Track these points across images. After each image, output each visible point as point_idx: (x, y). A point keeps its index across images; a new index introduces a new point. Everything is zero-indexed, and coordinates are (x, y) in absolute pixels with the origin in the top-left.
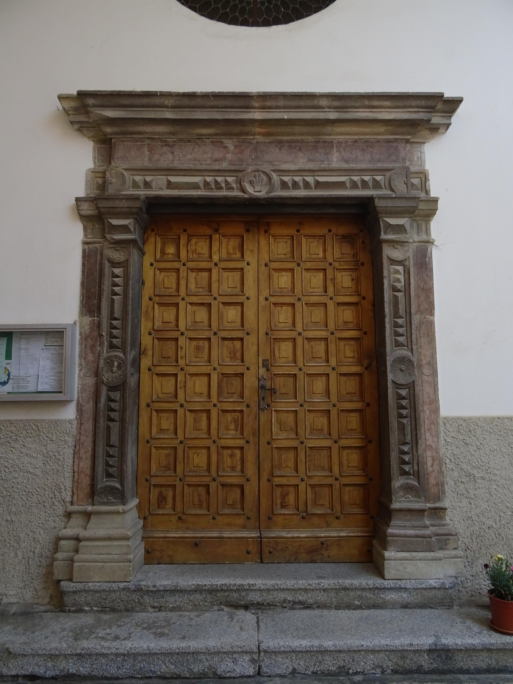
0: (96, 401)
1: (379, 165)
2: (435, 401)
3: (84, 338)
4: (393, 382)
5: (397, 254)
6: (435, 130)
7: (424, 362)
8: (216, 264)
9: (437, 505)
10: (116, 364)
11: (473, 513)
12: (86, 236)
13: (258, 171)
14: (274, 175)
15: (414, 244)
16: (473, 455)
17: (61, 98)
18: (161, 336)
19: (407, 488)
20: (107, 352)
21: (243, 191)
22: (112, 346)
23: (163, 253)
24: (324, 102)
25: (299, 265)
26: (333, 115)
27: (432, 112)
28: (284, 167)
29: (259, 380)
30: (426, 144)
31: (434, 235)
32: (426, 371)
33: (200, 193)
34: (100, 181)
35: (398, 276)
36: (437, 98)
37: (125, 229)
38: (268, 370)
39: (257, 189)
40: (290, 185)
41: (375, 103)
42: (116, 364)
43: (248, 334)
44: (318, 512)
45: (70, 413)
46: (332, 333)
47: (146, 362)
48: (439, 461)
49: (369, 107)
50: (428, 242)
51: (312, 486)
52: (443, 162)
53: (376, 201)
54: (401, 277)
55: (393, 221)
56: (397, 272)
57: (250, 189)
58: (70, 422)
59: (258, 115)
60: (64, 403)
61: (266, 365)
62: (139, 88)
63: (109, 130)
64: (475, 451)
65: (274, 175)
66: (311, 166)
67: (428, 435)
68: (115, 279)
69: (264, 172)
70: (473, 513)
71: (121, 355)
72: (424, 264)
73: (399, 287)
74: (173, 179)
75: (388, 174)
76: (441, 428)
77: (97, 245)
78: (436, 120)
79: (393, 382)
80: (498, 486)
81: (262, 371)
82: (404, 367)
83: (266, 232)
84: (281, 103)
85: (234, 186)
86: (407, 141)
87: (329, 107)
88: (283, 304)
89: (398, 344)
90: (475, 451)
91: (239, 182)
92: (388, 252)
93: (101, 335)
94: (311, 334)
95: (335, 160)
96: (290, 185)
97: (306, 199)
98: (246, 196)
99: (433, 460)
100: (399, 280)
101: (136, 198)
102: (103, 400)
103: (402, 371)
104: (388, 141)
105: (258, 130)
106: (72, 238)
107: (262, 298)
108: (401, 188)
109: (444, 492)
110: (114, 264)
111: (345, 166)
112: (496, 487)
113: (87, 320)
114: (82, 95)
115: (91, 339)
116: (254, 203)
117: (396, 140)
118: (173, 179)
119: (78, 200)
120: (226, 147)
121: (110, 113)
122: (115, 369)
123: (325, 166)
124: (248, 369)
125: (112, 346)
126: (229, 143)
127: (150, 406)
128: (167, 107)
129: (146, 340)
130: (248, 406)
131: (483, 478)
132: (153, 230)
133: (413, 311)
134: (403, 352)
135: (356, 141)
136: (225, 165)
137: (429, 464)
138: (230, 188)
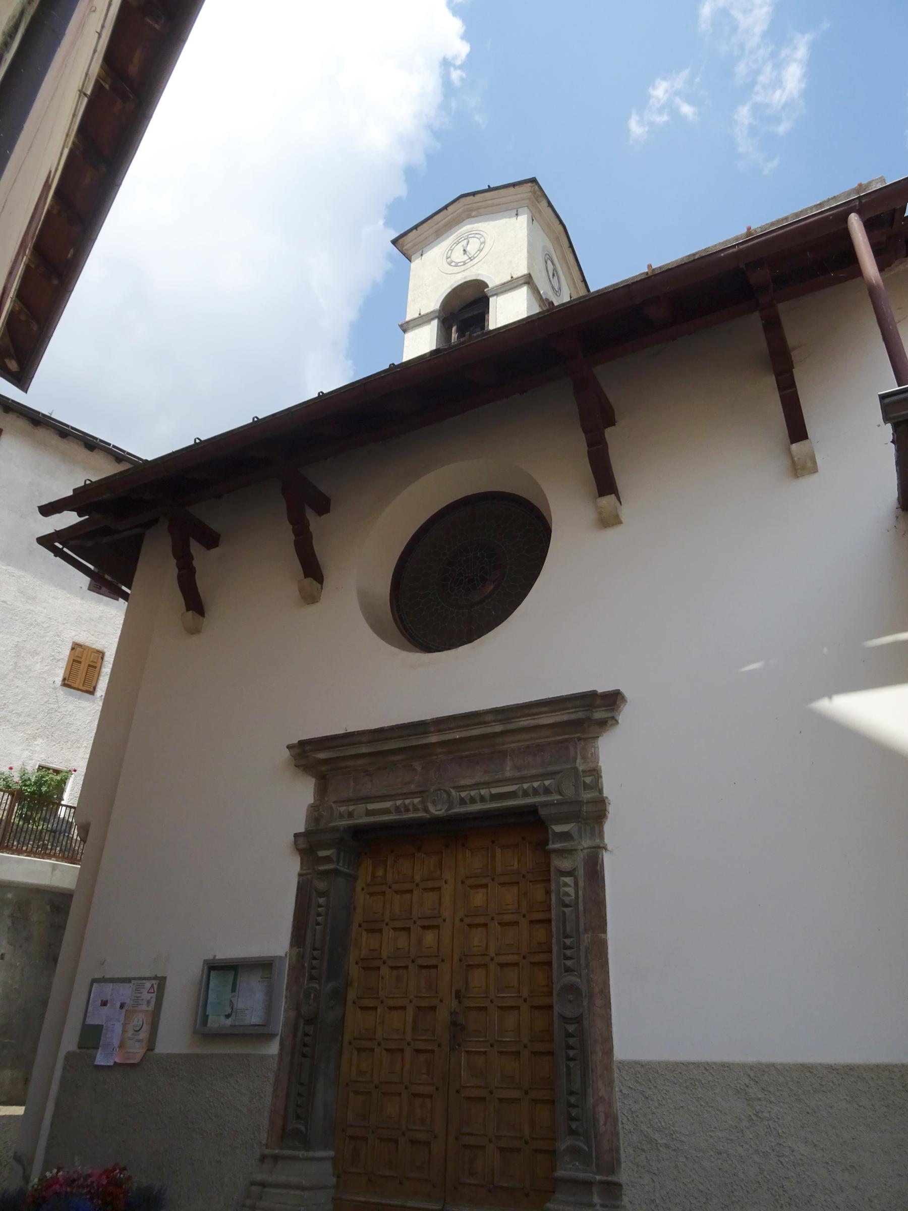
0: (295, 1036)
1: (550, 769)
2: (608, 1039)
3: (292, 969)
4: (560, 1015)
5: (565, 864)
6: (604, 724)
7: (596, 990)
8: (417, 885)
9: (610, 1178)
10: (312, 996)
11: (657, 1195)
12: (301, 868)
13: (439, 790)
14: (453, 792)
15: (585, 851)
16: (654, 1113)
17: (289, 747)
18: (370, 965)
19: (574, 1151)
20: (308, 984)
21: (426, 810)
22: (312, 978)
23: (374, 876)
24: (489, 718)
25: (493, 880)
26: (498, 728)
27: (595, 711)
28: (463, 782)
29: (451, 1014)
30: (600, 739)
31: (607, 839)
32: (599, 1002)
33: (391, 818)
34: (315, 813)
35: (567, 889)
36: (589, 700)
37: (328, 859)
38: (460, 1002)
39: (439, 808)
40: (468, 801)
41: (534, 711)
42: (312, 996)
43: (443, 961)
44: (505, 1185)
45: (274, 1048)
46: (524, 958)
47: (352, 995)
48: (612, 1118)
49: (529, 715)
50: (599, 847)
51: (502, 1150)
52: (615, 757)
53: (540, 809)
54: (571, 891)
55: (558, 828)
56: (566, 885)
57: (432, 809)
58: (273, 1056)
59: (434, 739)
60: (270, 1037)
61: (458, 995)
62: (340, 731)
63: (323, 768)
64: (656, 1108)
65: (453, 792)
66: (486, 778)
67: (600, 1084)
68: (320, 909)
69: (445, 791)
70: (657, 1195)
71: (317, 986)
72: (594, 873)
73: (567, 902)
74: (371, 806)
75: (558, 776)
76: (616, 1075)
77: (309, 876)
78: (598, 715)
79: (560, 1015)
80: (687, 1158)
81: (454, 1004)
82: (571, 997)
83: (463, 845)
84: (452, 725)
85: (420, 807)
86: (579, 739)
87: (494, 721)
88: (478, 925)
89: (568, 970)
90: (656, 1108)
91: (423, 802)
92: (559, 863)
93: (303, 967)
94: (503, 959)
95: (508, 769)
96: (468, 801)
97: (479, 812)
98: (428, 816)
99: (607, 1117)
100: (567, 894)
101: (335, 830)
102: (300, 1034)
103: (571, 1002)
104: (560, 742)
105: (439, 750)
106: (290, 869)
107: (457, 920)
108: (569, 792)
109: (619, 1162)
110: (321, 894)
111: (517, 774)
112: (684, 1160)
113: (296, 950)
114: (302, 743)
115: (296, 971)
116: (436, 822)
117: (567, 740)
118: (371, 806)
119: (296, 835)
120: (414, 770)
121: (321, 756)
122: (312, 1001)
123: (498, 776)
124: (441, 1001)
125: (312, 978)
126: (418, 766)
127: (107, 1002)
128: (363, 743)
129: (354, 971)
130: (439, 1045)
131: (667, 1146)
132: (366, 854)
133: (581, 928)
134: (571, 979)
135: (528, 747)
136: (413, 787)
137: (602, 1122)
138: (416, 810)
